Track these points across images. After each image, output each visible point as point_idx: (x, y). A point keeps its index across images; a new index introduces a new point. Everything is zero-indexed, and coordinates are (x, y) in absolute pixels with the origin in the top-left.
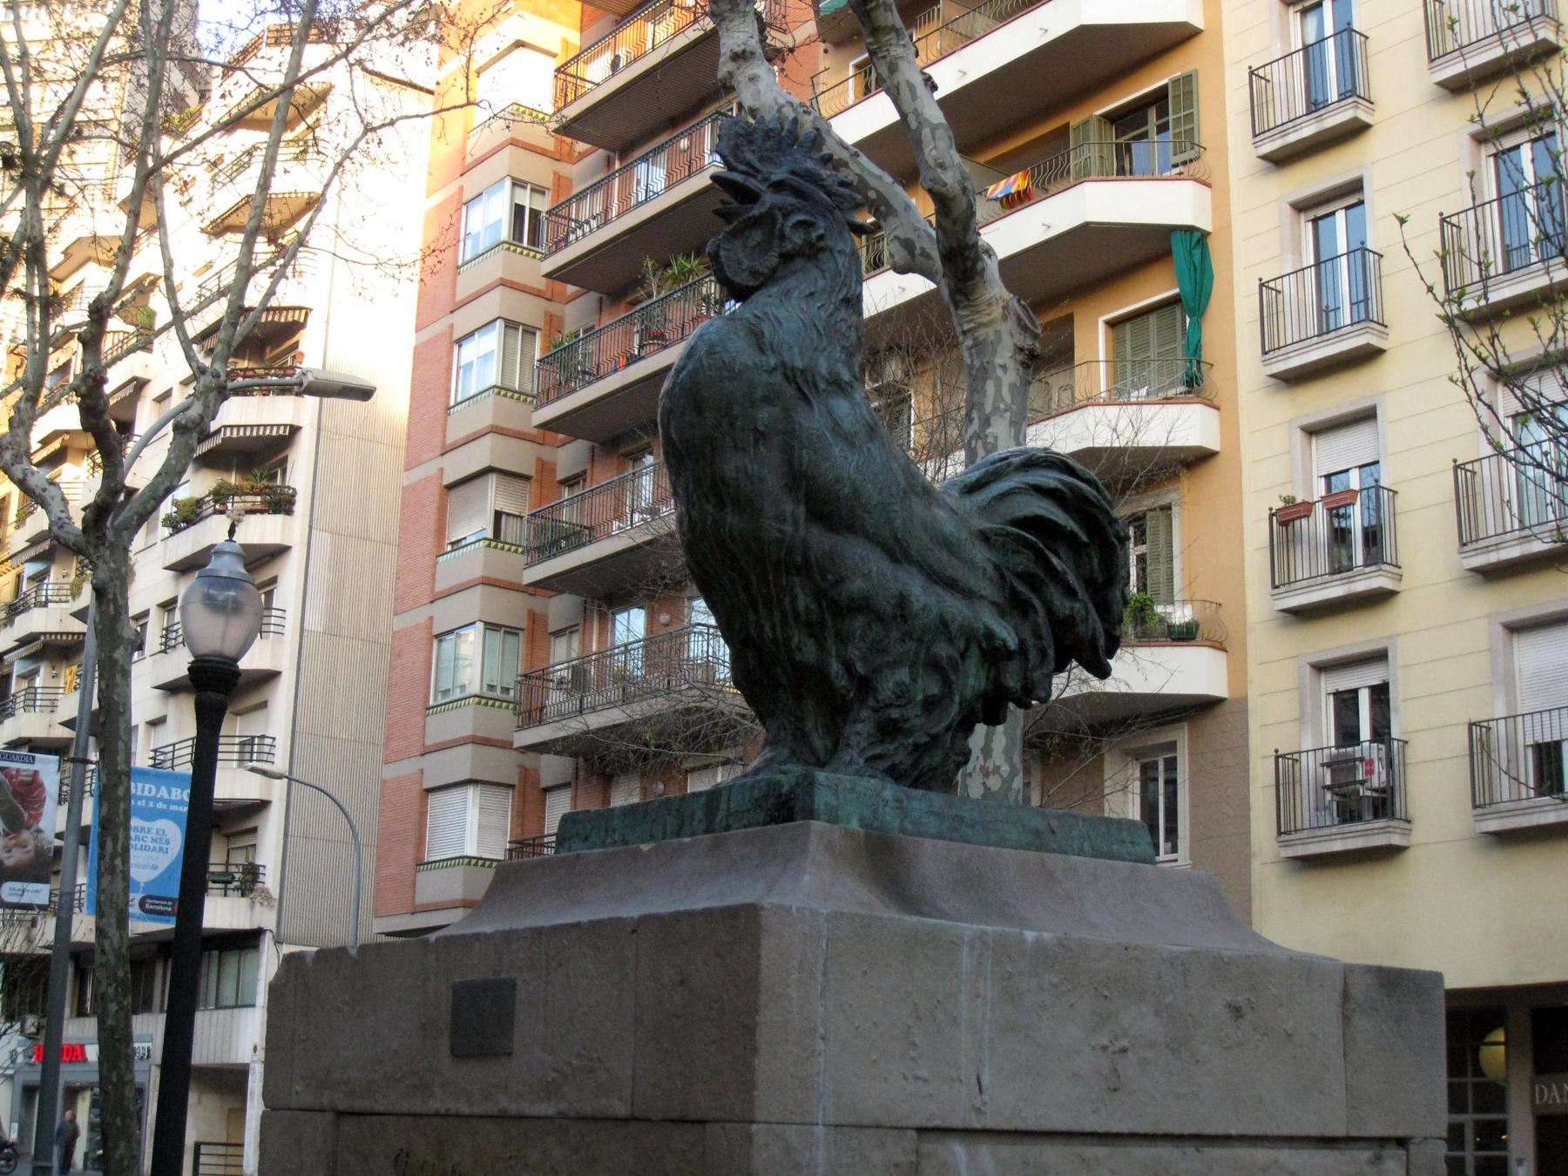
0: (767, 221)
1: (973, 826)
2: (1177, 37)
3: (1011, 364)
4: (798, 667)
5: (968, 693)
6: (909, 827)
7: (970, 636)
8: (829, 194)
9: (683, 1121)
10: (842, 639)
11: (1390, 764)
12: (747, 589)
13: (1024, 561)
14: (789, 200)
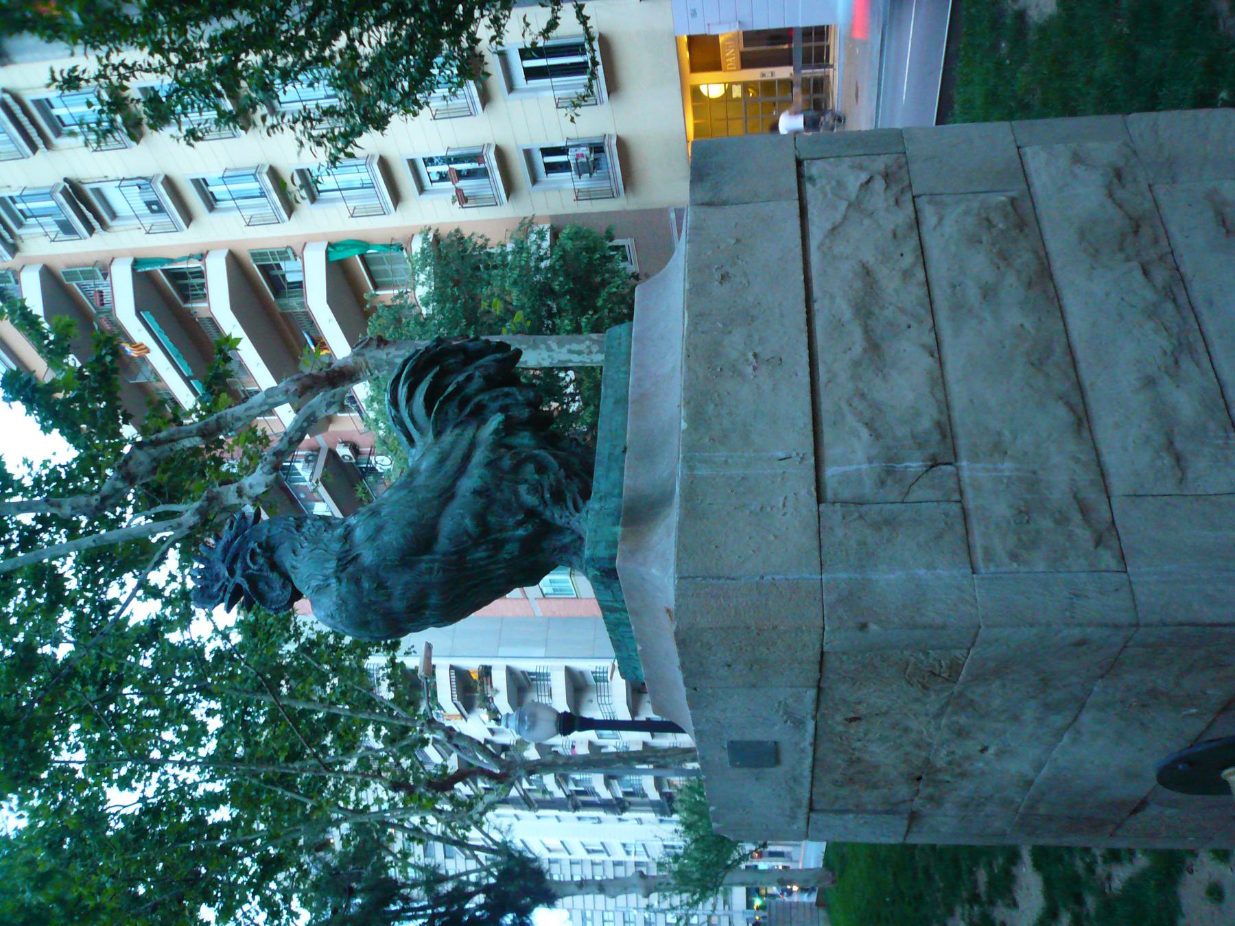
0: (251, 579)
3: (386, 351)
6: (616, 491)
8: (236, 538)
11: (578, 146)
13: (452, 409)
14: (238, 567)
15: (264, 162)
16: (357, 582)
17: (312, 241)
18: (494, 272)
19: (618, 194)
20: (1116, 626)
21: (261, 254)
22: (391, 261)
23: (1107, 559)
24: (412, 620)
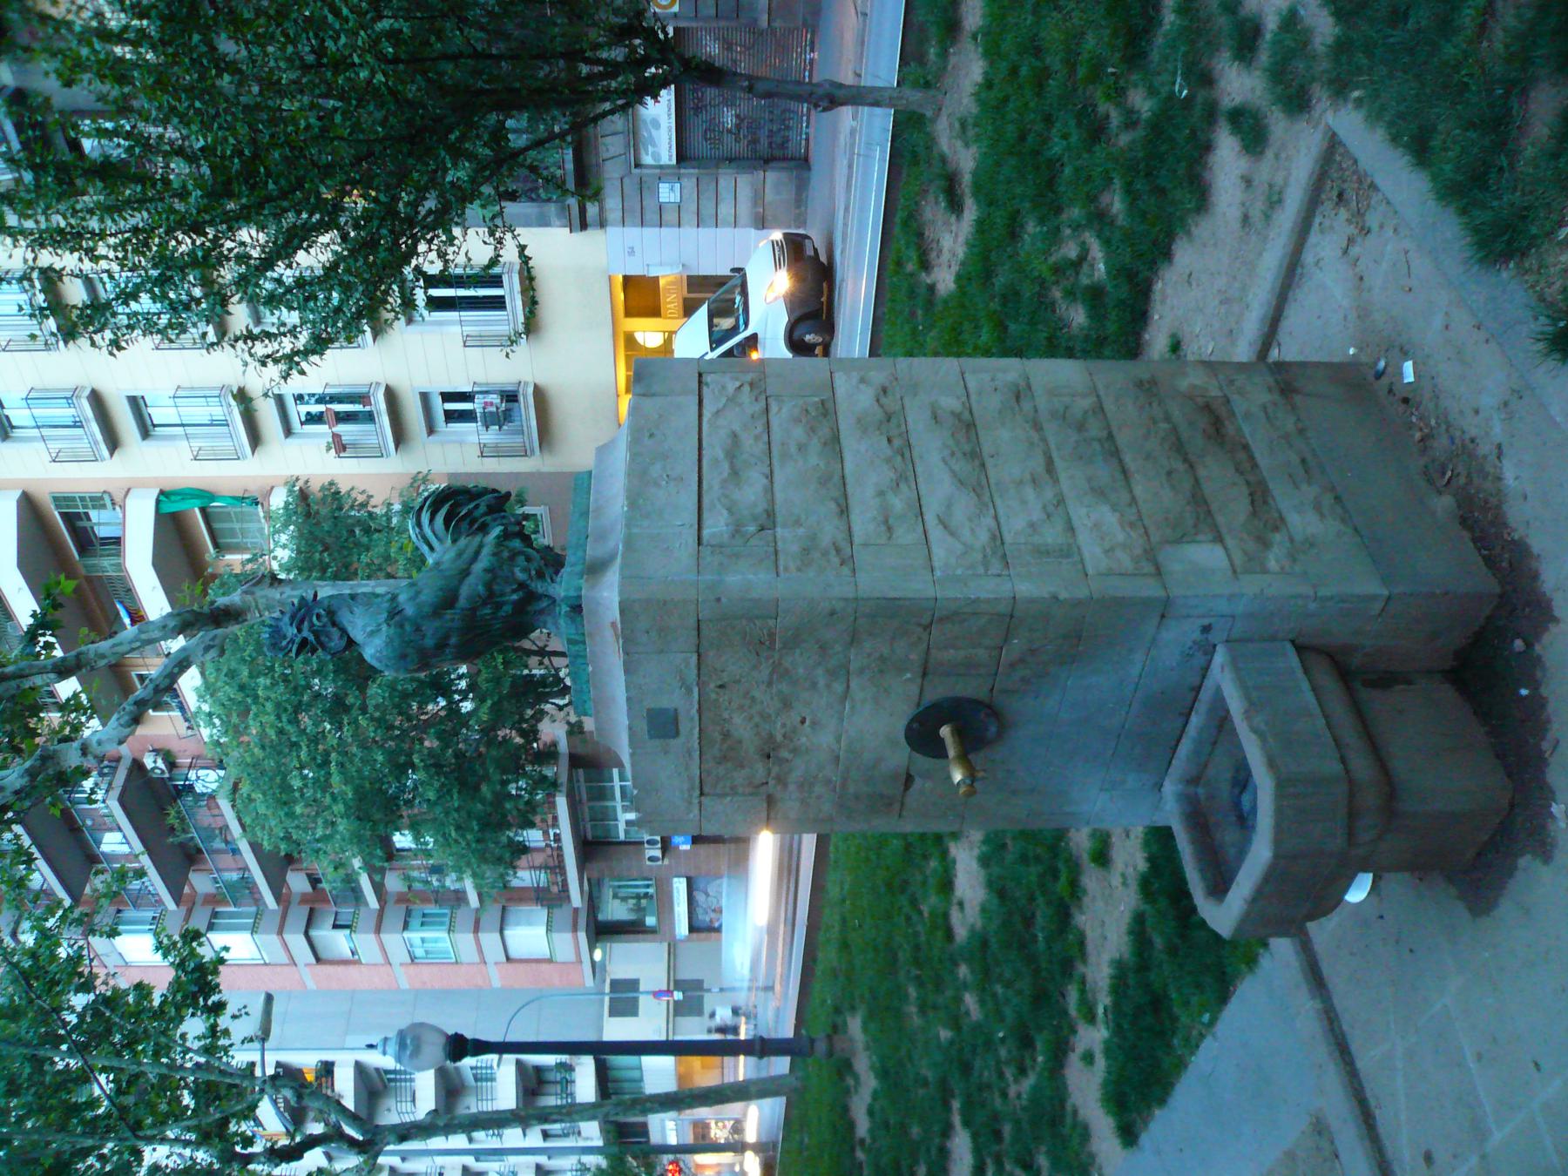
0: (316, 634)
2: (29, 507)
3: (280, 589)
4: (513, 614)
15: (86, 383)
16: (401, 626)
17: (138, 487)
18: (376, 536)
20: (846, 600)
21: (66, 499)
22: (241, 518)
23: (846, 570)
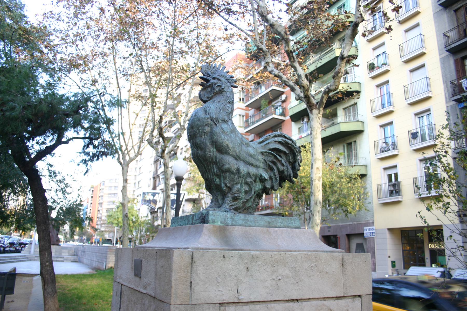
1: (251, 222)
4: (216, 185)
5: (257, 189)
7: (256, 176)
9: (161, 301)
10: (224, 178)
12: (205, 168)
13: (272, 158)
19: (379, 201)
24: (193, 145)
